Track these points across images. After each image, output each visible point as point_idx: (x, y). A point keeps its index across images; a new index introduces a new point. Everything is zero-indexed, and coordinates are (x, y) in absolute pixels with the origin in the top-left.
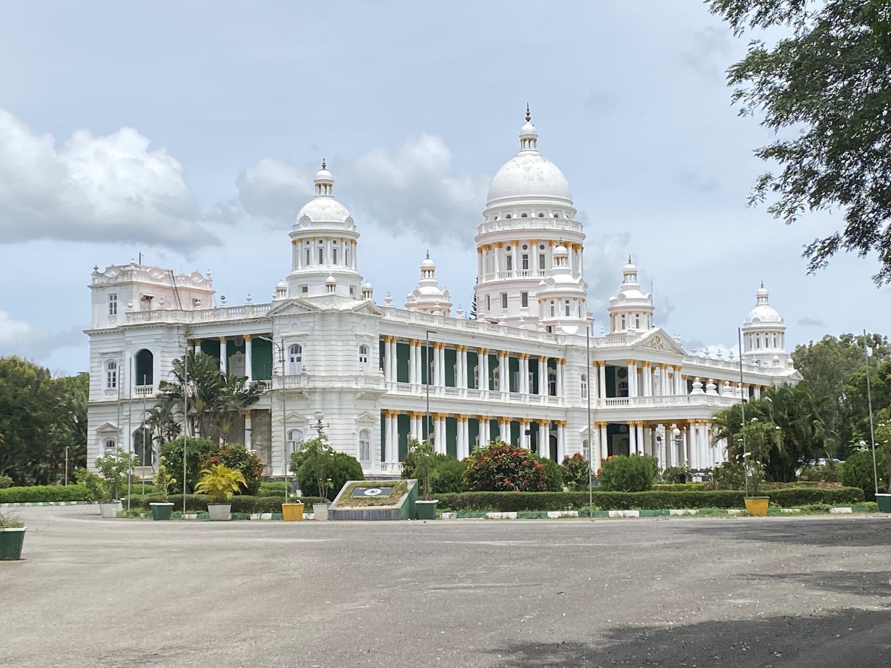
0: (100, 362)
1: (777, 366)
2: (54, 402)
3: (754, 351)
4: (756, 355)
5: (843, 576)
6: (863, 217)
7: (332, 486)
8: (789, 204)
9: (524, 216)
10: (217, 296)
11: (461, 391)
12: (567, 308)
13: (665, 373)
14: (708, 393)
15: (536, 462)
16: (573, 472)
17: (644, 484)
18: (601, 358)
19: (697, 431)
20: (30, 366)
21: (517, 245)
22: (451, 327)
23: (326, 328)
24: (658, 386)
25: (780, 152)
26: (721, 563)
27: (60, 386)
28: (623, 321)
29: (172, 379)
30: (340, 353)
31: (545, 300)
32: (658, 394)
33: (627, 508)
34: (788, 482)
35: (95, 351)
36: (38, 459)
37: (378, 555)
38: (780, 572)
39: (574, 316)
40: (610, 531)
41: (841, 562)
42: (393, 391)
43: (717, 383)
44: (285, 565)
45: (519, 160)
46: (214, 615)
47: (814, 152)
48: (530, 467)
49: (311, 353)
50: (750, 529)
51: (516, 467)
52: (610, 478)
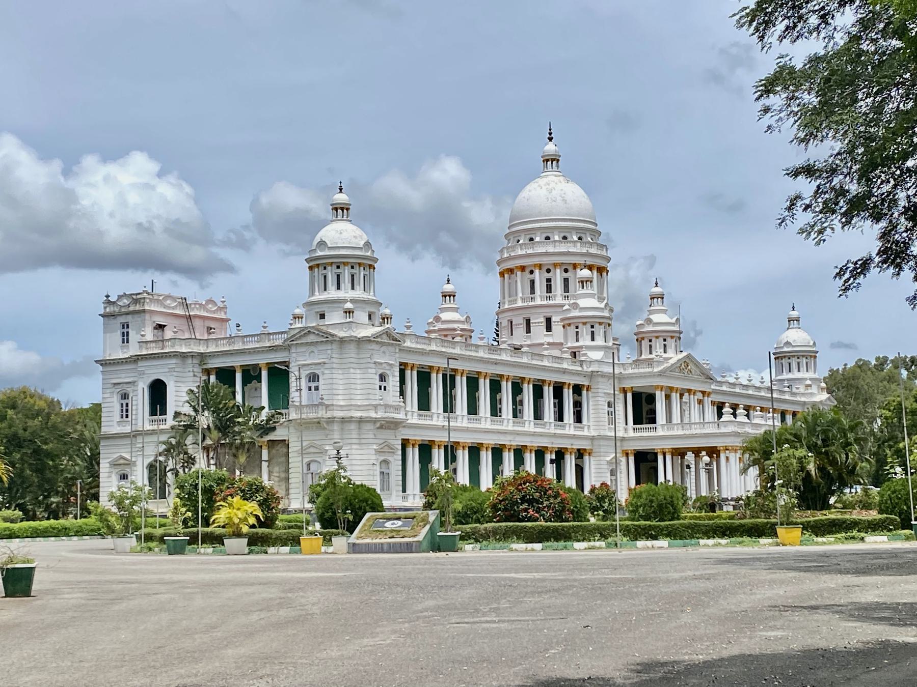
1: (810, 391)
3: (785, 376)
4: (788, 380)
5: (879, 607)
7: (351, 518)
9: (548, 238)
10: (232, 324)
11: (483, 419)
12: (593, 333)
13: (694, 399)
14: (739, 419)
15: (561, 492)
17: (674, 513)
18: (627, 385)
19: (727, 458)
20: (40, 397)
21: (540, 269)
22: (474, 354)
23: (345, 356)
24: (687, 413)
25: (809, 171)
26: (751, 594)
27: (71, 418)
28: (650, 346)
29: (187, 410)
31: (569, 325)
32: (686, 420)
33: (655, 538)
36: (49, 494)
37: (399, 589)
38: (813, 603)
39: (599, 341)
41: (877, 592)
42: (414, 420)
44: (303, 600)
45: (541, 181)
48: (555, 497)
50: (783, 559)
51: (541, 497)
52: (637, 507)
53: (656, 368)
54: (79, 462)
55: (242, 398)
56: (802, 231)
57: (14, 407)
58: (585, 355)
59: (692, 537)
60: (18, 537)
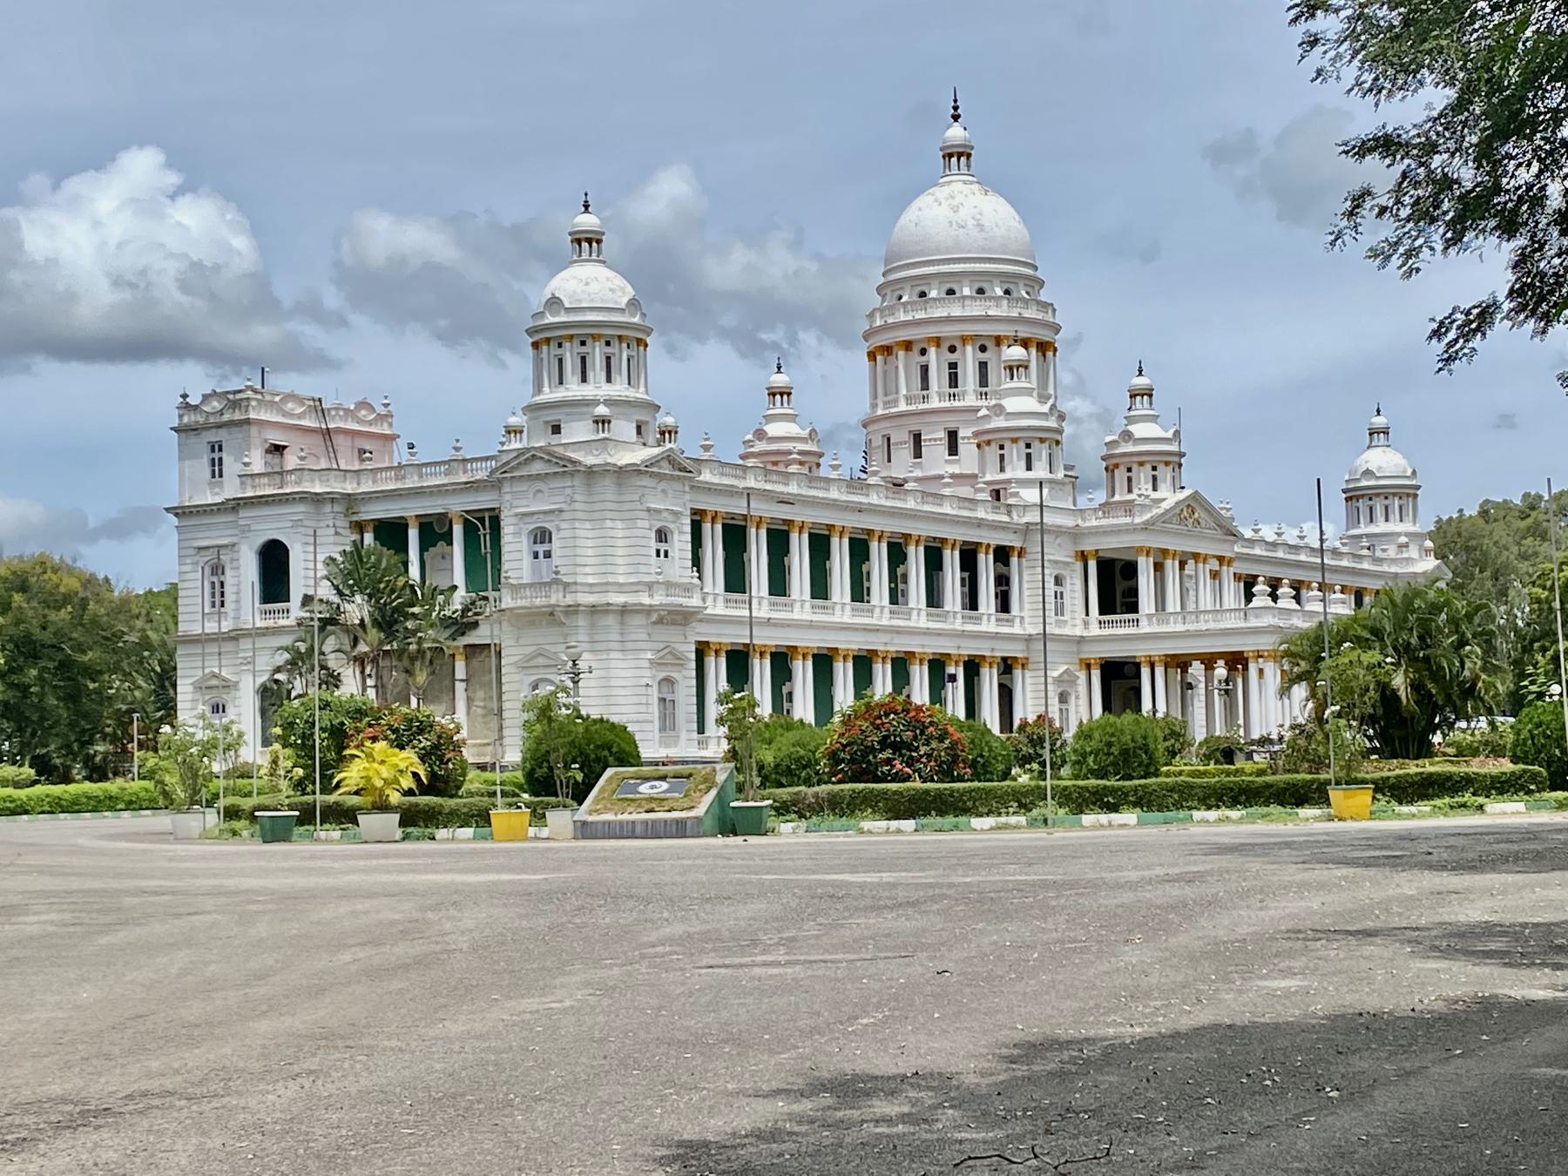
0: (197, 563)
1: (1405, 555)
2: (114, 635)
3: (1363, 529)
4: (1367, 536)
5: (1488, 930)
6: (1542, 265)
7: (579, 777)
8: (1407, 242)
9: (951, 292)
10: (402, 444)
11: (838, 607)
12: (1029, 456)
13: (1204, 570)
14: (1281, 603)
15: (951, 729)
16: (1034, 746)
17: (1148, 766)
18: (1088, 546)
19: (1261, 671)
20: (71, 571)
21: (938, 346)
22: (821, 494)
23: (596, 498)
24: (1192, 593)
25: (1386, 145)
26: (1261, 909)
27: (123, 607)
28: (1130, 479)
29: (325, 591)
30: (620, 543)
31: (989, 443)
32: (1191, 607)
33: (1113, 808)
34: (1417, 758)
35: (187, 544)
36: (92, 736)
37: (631, 903)
38: (1370, 924)
39: (1040, 471)
40: (1075, 853)
41: (1488, 904)
42: (718, 608)
43: (1297, 586)
44: (448, 926)
45: (940, 192)
46: (264, 1026)
47: (1451, 145)
48: (941, 739)
49: (570, 542)
50: (1332, 844)
51: (915, 738)
52: (1084, 755)
53: (1137, 517)
54: (141, 682)
55: (415, 574)
56: (1374, 253)
57: (23, 588)
58: (1016, 495)
59: (1178, 806)
60: (26, 812)
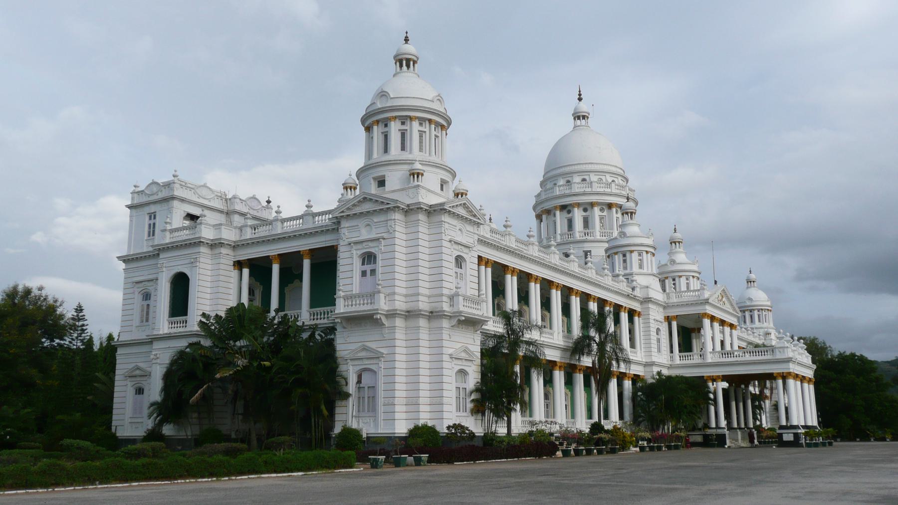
18: (673, 312)
